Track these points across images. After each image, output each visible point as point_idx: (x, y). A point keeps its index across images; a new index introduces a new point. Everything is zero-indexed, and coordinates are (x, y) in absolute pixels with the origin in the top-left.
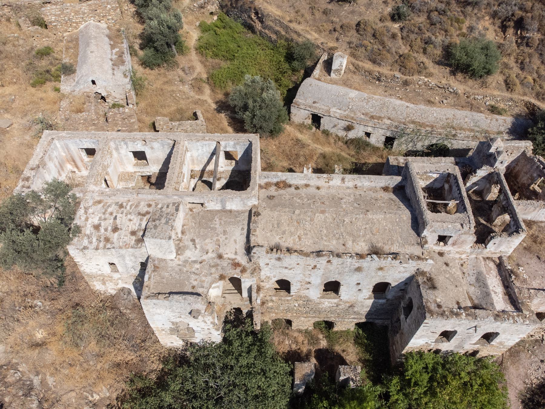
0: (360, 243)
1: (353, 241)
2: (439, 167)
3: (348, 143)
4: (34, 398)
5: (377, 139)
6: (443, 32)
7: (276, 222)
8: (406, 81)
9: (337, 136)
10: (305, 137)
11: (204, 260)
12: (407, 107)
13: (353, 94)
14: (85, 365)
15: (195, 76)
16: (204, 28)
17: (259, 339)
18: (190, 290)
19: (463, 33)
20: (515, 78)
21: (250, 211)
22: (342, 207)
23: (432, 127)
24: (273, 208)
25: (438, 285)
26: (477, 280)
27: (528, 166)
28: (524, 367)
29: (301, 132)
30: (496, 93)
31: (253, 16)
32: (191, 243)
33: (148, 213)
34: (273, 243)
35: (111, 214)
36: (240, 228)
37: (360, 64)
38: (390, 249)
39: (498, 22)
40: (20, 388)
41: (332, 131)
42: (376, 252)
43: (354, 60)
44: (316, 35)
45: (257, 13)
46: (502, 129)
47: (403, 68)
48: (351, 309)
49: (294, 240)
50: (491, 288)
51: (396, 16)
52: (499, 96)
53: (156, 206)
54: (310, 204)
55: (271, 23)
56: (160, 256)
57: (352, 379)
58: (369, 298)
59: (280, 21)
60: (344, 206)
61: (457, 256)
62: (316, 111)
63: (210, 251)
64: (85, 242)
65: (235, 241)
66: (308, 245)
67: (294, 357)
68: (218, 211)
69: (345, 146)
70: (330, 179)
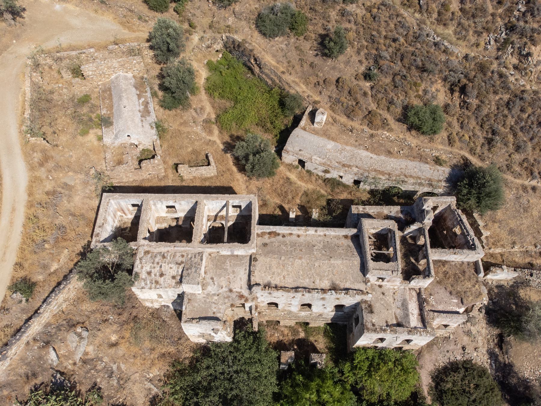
0: (325, 281)
1: (320, 280)
2: (384, 224)
3: (326, 181)
4: (115, 378)
5: (348, 180)
6: (404, 93)
7: (268, 266)
8: (372, 134)
9: (317, 175)
10: (293, 177)
11: (220, 293)
12: (371, 158)
13: (330, 145)
14: (143, 356)
15: (205, 117)
16: (210, 66)
17: (256, 336)
18: (212, 315)
19: (419, 95)
20: (455, 135)
21: (251, 256)
22: (314, 254)
23: (389, 174)
24: (266, 254)
25: (375, 310)
26: (403, 305)
27: (452, 216)
28: (435, 355)
29: (290, 171)
30: (440, 147)
31: (252, 61)
32: (211, 281)
33: (182, 262)
34: (266, 282)
35: (158, 263)
36: (244, 269)
37: (338, 117)
38: (344, 285)
39: (448, 86)
40: (106, 373)
41: (315, 171)
42: (334, 288)
43: (333, 114)
44: (304, 87)
45: (255, 60)
46: (441, 178)
47: (370, 124)
48: (320, 317)
50: (410, 311)
51: (367, 76)
52: (442, 149)
53: (187, 256)
54: (292, 251)
55: (267, 71)
56: (191, 292)
57: (319, 363)
58: (332, 311)
59: (275, 72)
60: (315, 253)
61: (392, 287)
62: (301, 158)
63: (224, 286)
64: (143, 284)
65: (241, 279)
66: (290, 282)
67: (280, 346)
68: (228, 256)
69: (323, 184)
70: (306, 231)
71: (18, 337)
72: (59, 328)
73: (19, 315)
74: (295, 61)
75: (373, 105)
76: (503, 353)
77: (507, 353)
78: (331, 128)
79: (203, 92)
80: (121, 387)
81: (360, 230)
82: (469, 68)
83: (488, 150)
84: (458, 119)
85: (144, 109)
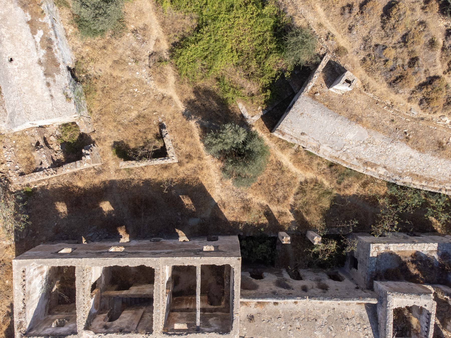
12: (411, 157)
75: (439, 66)
81: (383, 299)
85: (47, 55)
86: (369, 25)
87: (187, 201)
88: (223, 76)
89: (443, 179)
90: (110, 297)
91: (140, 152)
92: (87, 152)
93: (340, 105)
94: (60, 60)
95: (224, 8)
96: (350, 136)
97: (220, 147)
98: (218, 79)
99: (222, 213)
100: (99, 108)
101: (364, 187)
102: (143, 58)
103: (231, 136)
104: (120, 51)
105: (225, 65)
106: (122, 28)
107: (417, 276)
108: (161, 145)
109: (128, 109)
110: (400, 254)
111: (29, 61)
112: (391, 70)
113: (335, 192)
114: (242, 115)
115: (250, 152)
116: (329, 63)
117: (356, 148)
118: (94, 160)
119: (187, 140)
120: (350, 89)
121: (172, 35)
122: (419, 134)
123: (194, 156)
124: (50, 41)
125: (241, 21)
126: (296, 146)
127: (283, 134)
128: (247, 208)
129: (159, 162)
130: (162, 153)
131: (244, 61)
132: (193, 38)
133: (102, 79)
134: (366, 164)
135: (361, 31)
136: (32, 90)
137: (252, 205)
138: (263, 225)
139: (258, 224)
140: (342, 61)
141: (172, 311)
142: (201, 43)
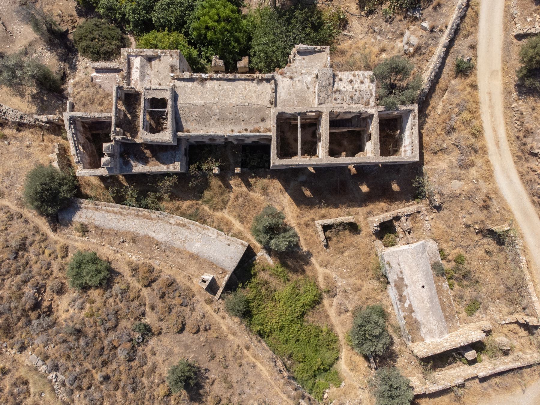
1: (214, 88)
6: (107, 305)
12: (154, 232)
25: (169, 67)
26: (144, 77)
32: (309, 86)
49: (249, 87)
50: (139, 71)
63: (297, 82)
65: (284, 89)
71: (454, 25)
72: (427, 45)
73: (460, 47)
74: (233, 364)
75: (145, 294)
76: (64, 69)
77: (61, 68)
78: (195, 272)
79: (341, 337)
80: (371, 27)
81: (175, 135)
82: (23, 332)
83: (27, 238)
84: (52, 274)
85: (402, 291)
86: (192, 319)
87: (308, 193)
88: (285, 282)
89: (129, 217)
90: (360, 127)
91: (341, 228)
92: (376, 228)
93: (205, 266)
94: (394, 288)
95: (286, 328)
96: (198, 245)
97: (288, 234)
98: (288, 280)
99: (282, 185)
100: (371, 257)
101: (179, 206)
102: (341, 293)
103: (280, 243)
104: (356, 297)
105: (283, 290)
106: (355, 312)
107: (146, 148)
108: (327, 233)
109: (350, 257)
110: (157, 162)
111: (412, 287)
112: (176, 290)
113: (200, 202)
114: (270, 255)
115: (266, 233)
116: (215, 294)
117: (193, 237)
118: (372, 222)
119: (308, 237)
120: (203, 276)
121: (321, 310)
122: (149, 248)
123: (304, 226)
124: (400, 301)
125: (274, 321)
126: (229, 235)
127: (242, 244)
128: (265, 190)
129: (328, 221)
130: (326, 228)
131: (271, 293)
132: (306, 308)
133: (369, 277)
134: (184, 226)
135: (197, 315)
136: (411, 268)
137: (261, 191)
138: (253, 177)
139: (256, 178)
140: (209, 295)
141: (316, 119)
142: (301, 304)
